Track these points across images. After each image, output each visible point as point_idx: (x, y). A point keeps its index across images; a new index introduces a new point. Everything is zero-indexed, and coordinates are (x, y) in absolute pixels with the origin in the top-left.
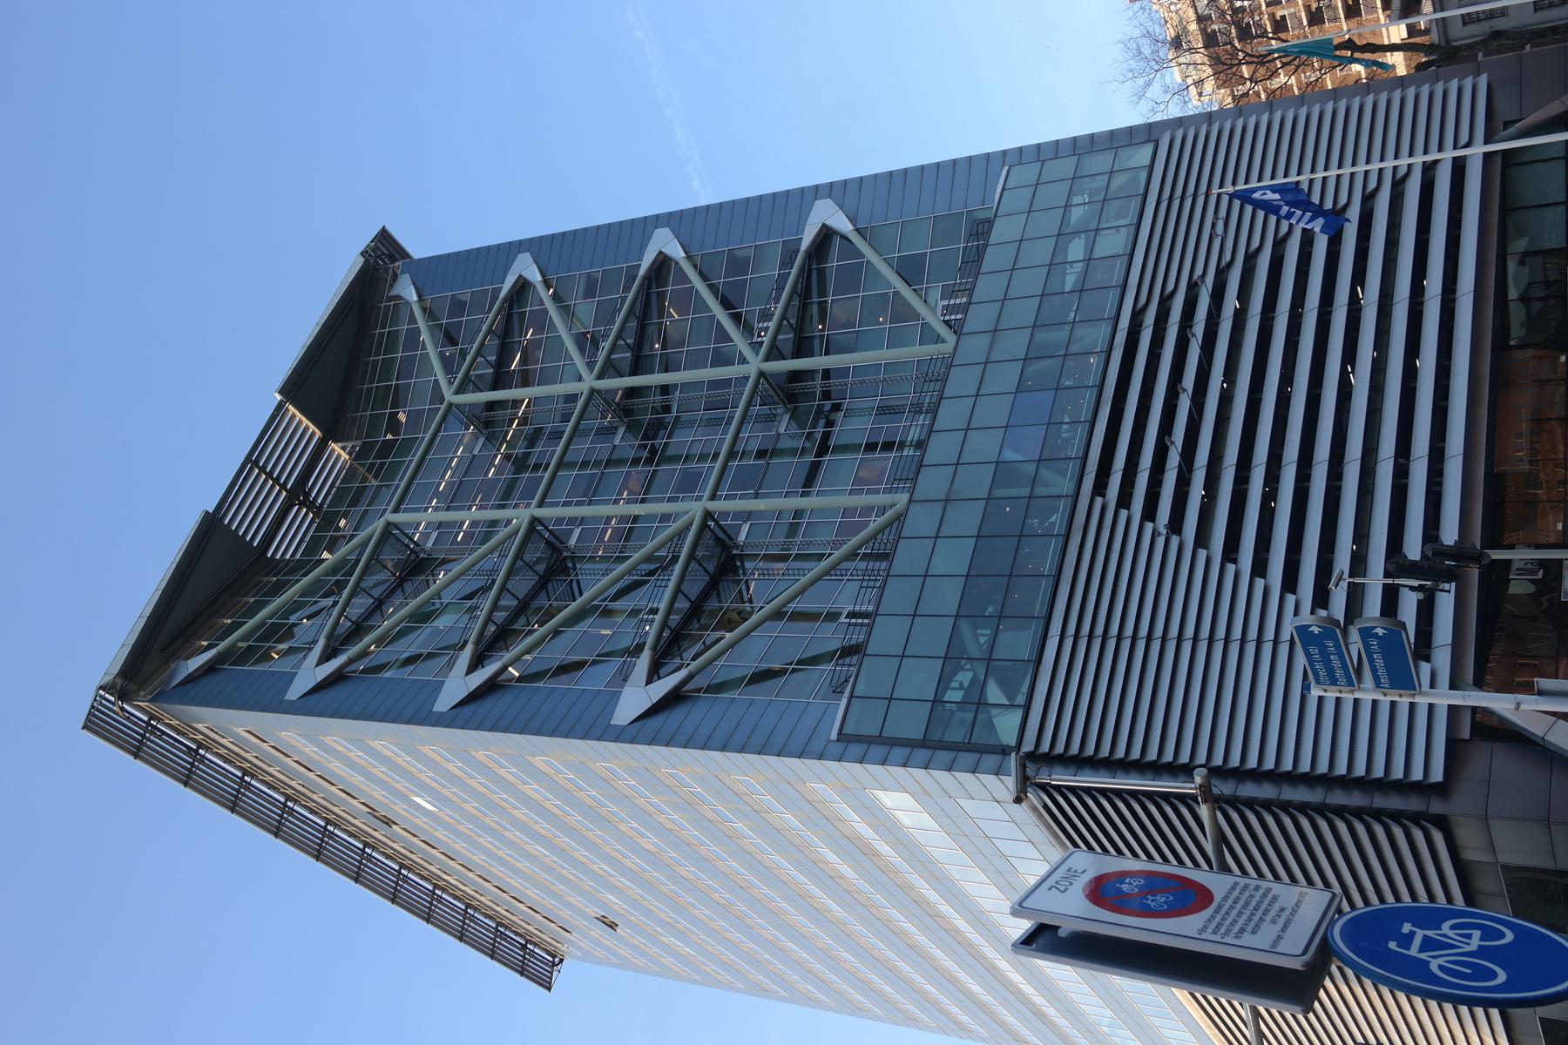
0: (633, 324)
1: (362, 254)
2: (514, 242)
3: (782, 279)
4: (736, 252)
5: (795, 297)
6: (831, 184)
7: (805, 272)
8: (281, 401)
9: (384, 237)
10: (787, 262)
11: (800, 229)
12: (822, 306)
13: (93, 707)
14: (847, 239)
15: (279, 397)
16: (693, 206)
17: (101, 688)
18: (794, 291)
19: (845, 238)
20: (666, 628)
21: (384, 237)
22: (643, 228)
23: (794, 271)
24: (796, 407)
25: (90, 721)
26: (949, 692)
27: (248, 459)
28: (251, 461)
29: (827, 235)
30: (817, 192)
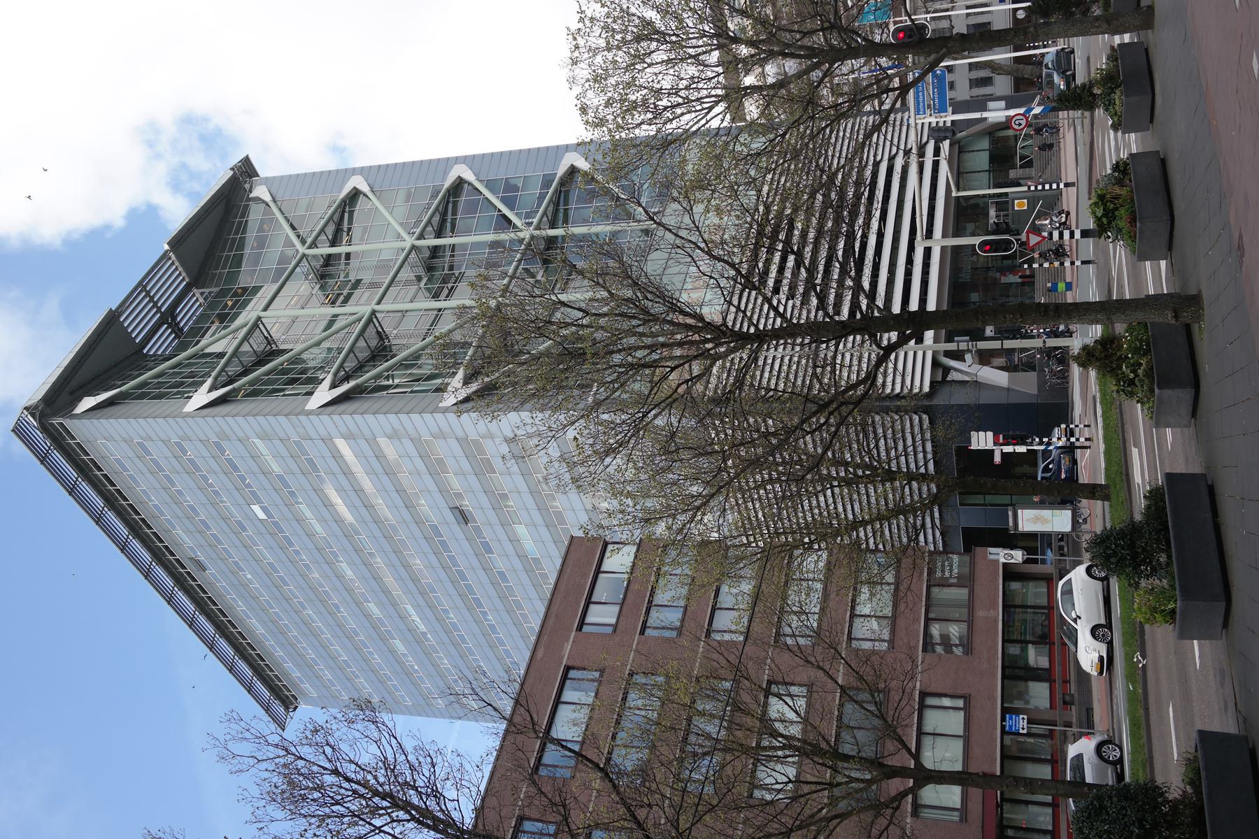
0: (551, 208)
1: (232, 169)
2: (442, 159)
3: (541, 198)
4: (510, 180)
5: (437, 214)
6: (466, 157)
7: (558, 192)
8: (167, 251)
9: (247, 161)
10: (434, 196)
11: (444, 179)
12: (566, 211)
13: (19, 420)
14: (267, 205)
15: (167, 247)
16: (473, 153)
17: (25, 408)
18: (551, 200)
19: (470, 184)
20: (949, 378)
21: (247, 161)
22: (449, 162)
23: (551, 191)
24: (547, 267)
25: (17, 428)
26: (394, 415)
27: (140, 283)
28: (142, 286)
29: (573, 170)
30: (457, 160)
